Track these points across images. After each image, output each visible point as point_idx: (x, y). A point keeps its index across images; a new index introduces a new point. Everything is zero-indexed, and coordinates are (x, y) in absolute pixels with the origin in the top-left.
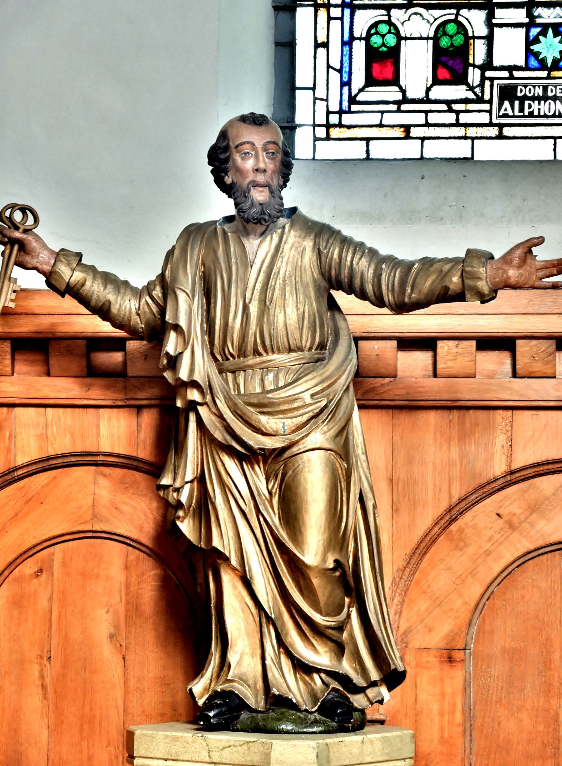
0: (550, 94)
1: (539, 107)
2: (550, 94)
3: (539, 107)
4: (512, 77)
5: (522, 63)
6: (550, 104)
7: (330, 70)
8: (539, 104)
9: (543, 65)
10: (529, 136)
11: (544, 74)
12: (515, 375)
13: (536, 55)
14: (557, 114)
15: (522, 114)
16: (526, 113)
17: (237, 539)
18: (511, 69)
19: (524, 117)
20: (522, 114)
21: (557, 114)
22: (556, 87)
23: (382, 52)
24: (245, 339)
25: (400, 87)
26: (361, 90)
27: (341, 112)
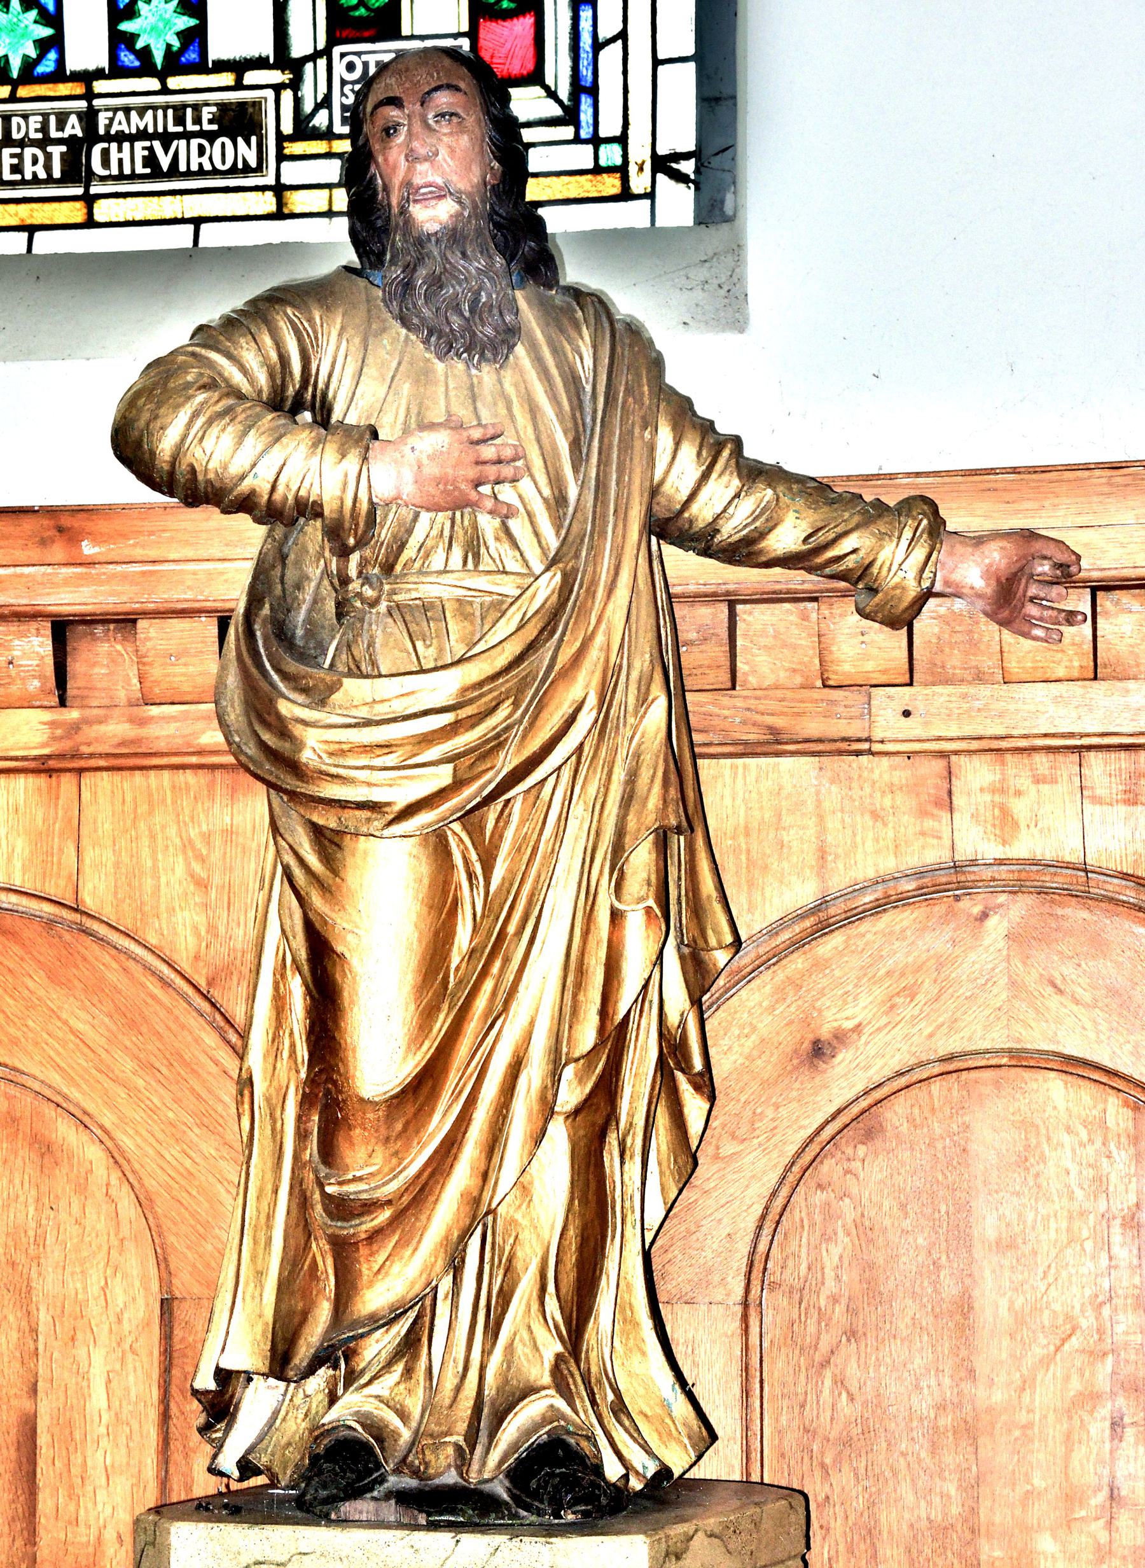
0: (16, 136)
1: (120, 155)
2: (16, 136)
3: (120, 155)
4: (239, 86)
5: (104, 62)
6: (223, 145)
7: (620, 42)
8: (120, 150)
9: (146, 68)
10: (229, 214)
11: (153, 84)
12: (911, 684)
13: (129, 39)
14: (240, 166)
15: (18, 177)
16: (28, 176)
17: (613, 999)
18: (239, 67)
19: (24, 182)
20: (18, 177)
21: (240, 166)
22: (25, 117)
23: (360, 17)
24: (99, 630)
25: (547, 88)
26: (552, 94)
27: (596, 141)
